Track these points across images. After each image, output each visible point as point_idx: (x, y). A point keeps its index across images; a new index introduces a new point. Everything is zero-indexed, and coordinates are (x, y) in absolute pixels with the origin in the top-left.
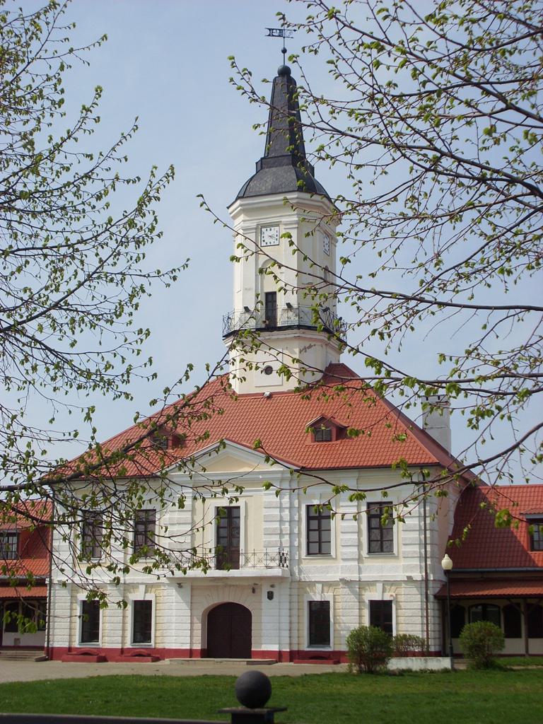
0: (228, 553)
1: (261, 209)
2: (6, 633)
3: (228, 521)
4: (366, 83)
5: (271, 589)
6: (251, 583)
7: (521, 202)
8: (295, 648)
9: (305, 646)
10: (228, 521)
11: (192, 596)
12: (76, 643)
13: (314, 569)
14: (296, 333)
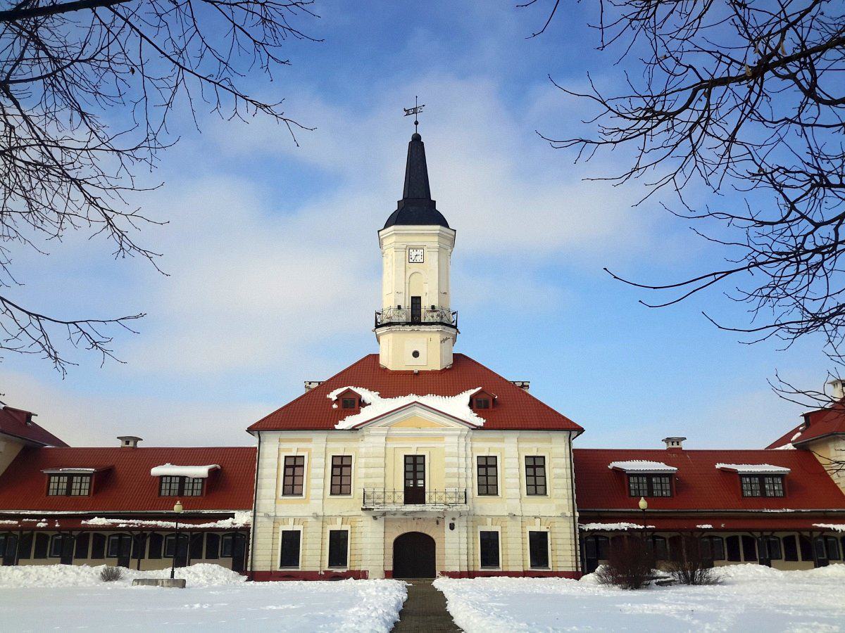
0: (415, 494)
1: (410, 234)
2: (133, 560)
3: (415, 466)
4: (599, 144)
5: (452, 522)
6: (435, 516)
7: (788, 222)
8: (471, 569)
9: (528, 568)
10: (415, 466)
11: (385, 527)
12: (528, 568)
13: (487, 505)
14: (440, 328)
